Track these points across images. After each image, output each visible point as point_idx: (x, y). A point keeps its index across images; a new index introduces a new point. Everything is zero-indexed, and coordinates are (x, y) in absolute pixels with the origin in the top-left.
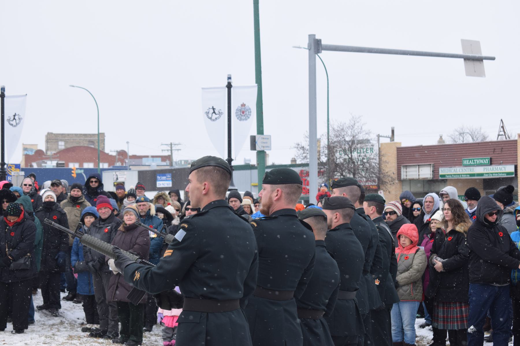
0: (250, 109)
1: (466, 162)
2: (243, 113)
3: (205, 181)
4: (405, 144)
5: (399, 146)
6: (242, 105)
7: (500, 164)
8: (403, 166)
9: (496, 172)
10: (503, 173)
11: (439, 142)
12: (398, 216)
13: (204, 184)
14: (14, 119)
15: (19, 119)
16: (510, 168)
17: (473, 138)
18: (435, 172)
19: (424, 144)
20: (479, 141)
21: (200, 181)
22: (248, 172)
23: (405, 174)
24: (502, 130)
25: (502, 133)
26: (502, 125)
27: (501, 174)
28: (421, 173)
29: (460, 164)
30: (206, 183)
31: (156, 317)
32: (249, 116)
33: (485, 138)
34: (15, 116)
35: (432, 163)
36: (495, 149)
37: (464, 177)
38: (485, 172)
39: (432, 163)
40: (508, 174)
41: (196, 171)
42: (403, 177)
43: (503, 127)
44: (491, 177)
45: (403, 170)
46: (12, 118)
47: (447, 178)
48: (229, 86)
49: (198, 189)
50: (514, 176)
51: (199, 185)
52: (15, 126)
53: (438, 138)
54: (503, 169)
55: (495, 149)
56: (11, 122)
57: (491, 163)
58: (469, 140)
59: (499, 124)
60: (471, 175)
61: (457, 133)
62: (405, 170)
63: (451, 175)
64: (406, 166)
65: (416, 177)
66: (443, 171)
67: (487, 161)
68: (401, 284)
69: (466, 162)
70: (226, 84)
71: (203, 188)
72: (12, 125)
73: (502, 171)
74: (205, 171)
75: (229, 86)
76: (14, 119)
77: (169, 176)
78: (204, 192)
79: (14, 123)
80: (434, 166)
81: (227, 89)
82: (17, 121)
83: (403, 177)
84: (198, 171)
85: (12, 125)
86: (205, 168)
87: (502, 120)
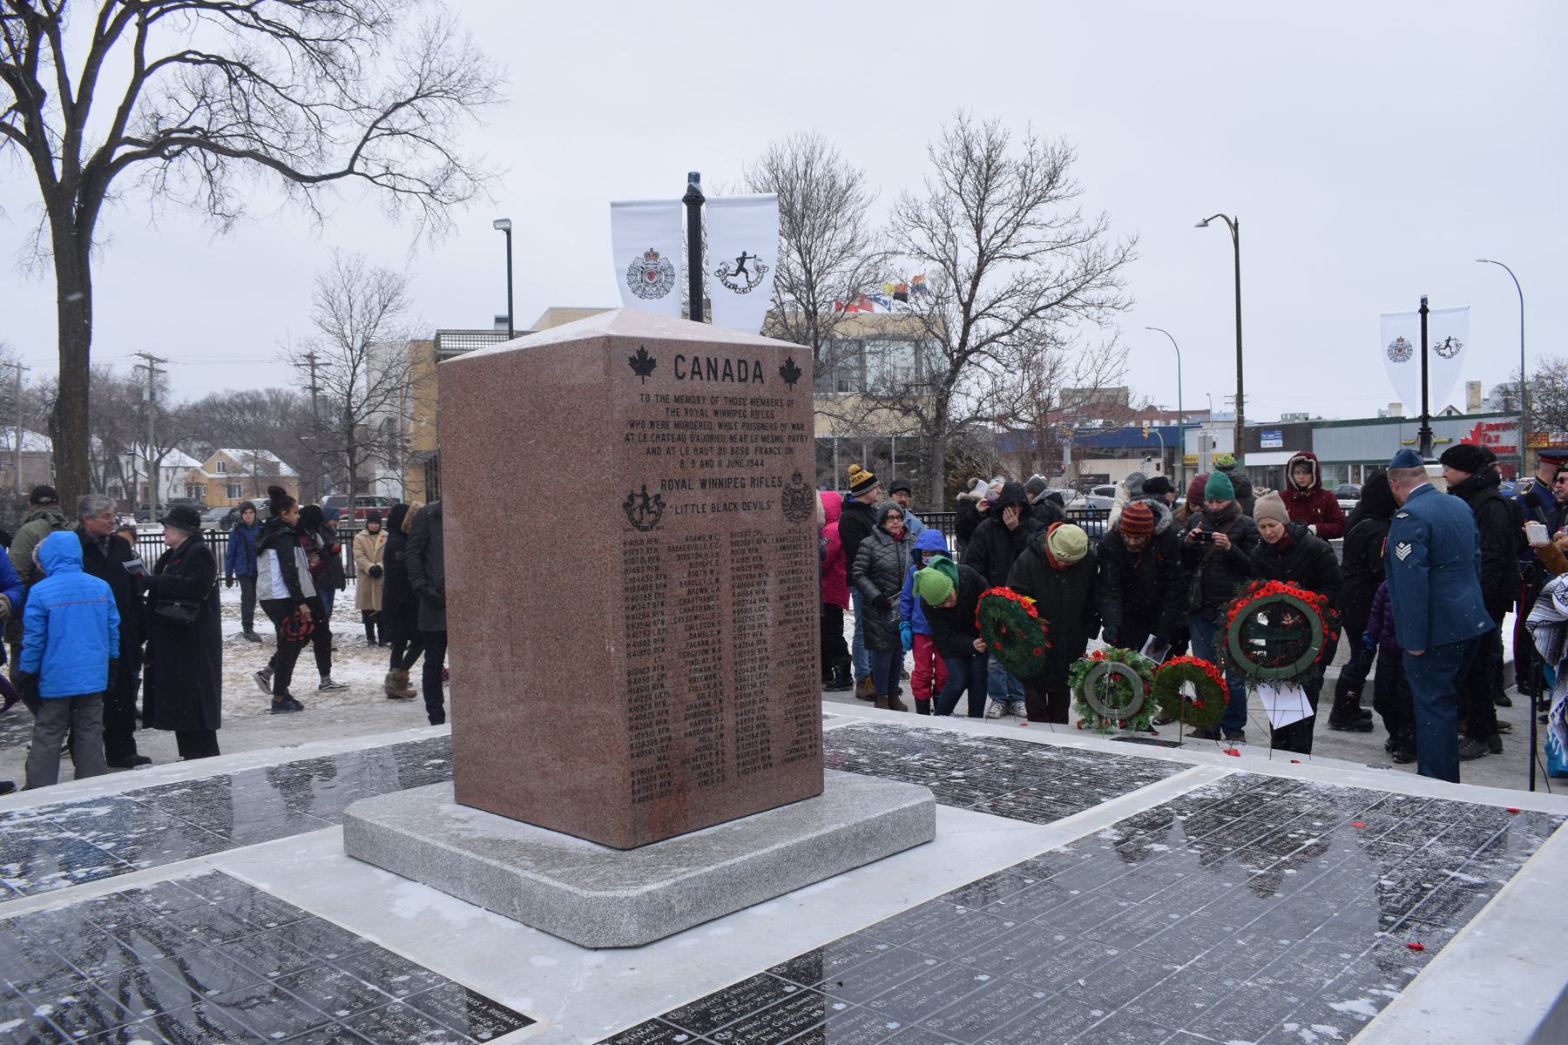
0: (671, 267)
2: (651, 275)
6: (647, 255)
14: (741, 269)
15: (758, 269)
22: (1396, 426)
32: (667, 286)
34: (742, 260)
46: (734, 267)
48: (1424, 311)
52: (744, 291)
56: (731, 280)
70: (684, 192)
72: (735, 287)
75: (1424, 311)
76: (741, 269)
77: (1278, 433)
79: (740, 280)
81: (685, 208)
82: (752, 277)
85: (735, 287)
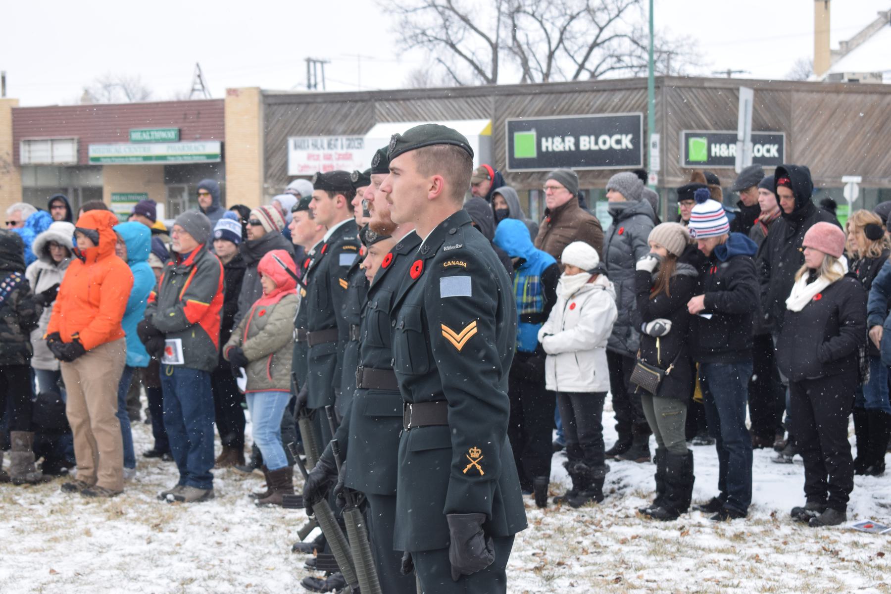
1: (135, 136)
3: (435, 172)
4: (28, 101)
5: (15, 105)
7: (195, 139)
8: (25, 141)
9: (189, 153)
10: (200, 155)
11: (83, 99)
12: (265, 231)
13: (433, 178)
16: (213, 148)
17: (128, 95)
18: (82, 151)
19: (61, 103)
20: (137, 99)
21: (424, 172)
23: (27, 154)
24: (198, 81)
25: (199, 87)
26: (198, 73)
27: (197, 158)
28: (49, 154)
29: (125, 138)
30: (439, 176)
31: (856, 434)
33: (145, 94)
35: (76, 137)
36: (185, 114)
37: (133, 162)
38: (171, 152)
39: (76, 137)
40: (209, 156)
41: (414, 152)
42: (24, 159)
43: (199, 76)
44: (180, 161)
45: (23, 148)
47: (103, 162)
49: (419, 187)
50: (218, 160)
51: (420, 180)
53: (81, 93)
54: (201, 148)
55: (185, 114)
57: (180, 137)
58: (120, 98)
59: (192, 72)
60: (146, 158)
61: (99, 86)
62: (27, 147)
63: (110, 158)
64: (29, 141)
65: (47, 160)
66: (96, 151)
67: (172, 134)
68: (86, 347)
69: (135, 136)
71: (430, 186)
73: (199, 153)
74: (436, 154)
78: (432, 194)
80: (80, 142)
83: (24, 159)
84: (420, 153)
86: (435, 148)
87: (198, 65)
